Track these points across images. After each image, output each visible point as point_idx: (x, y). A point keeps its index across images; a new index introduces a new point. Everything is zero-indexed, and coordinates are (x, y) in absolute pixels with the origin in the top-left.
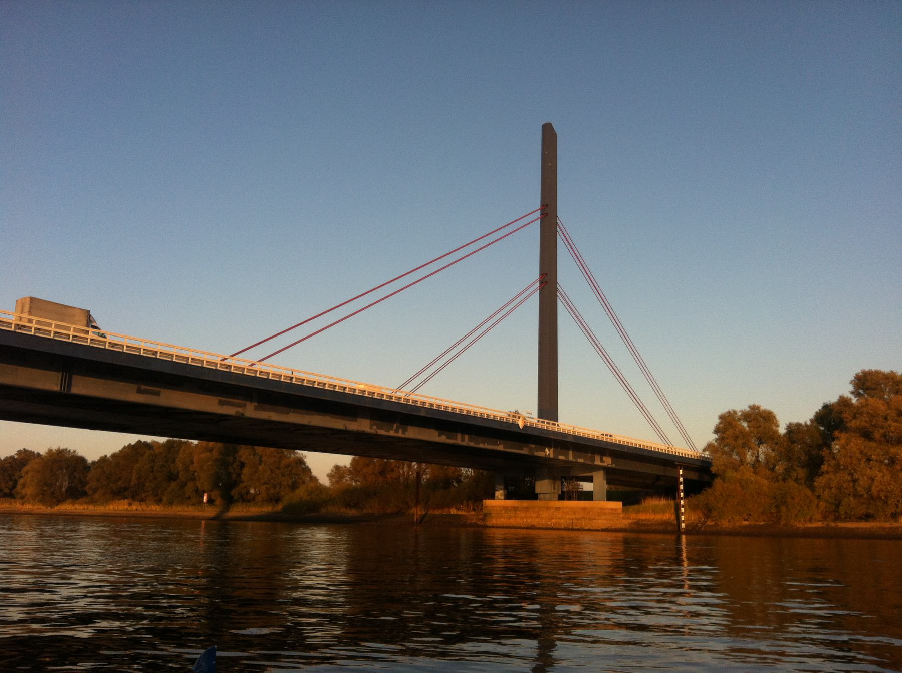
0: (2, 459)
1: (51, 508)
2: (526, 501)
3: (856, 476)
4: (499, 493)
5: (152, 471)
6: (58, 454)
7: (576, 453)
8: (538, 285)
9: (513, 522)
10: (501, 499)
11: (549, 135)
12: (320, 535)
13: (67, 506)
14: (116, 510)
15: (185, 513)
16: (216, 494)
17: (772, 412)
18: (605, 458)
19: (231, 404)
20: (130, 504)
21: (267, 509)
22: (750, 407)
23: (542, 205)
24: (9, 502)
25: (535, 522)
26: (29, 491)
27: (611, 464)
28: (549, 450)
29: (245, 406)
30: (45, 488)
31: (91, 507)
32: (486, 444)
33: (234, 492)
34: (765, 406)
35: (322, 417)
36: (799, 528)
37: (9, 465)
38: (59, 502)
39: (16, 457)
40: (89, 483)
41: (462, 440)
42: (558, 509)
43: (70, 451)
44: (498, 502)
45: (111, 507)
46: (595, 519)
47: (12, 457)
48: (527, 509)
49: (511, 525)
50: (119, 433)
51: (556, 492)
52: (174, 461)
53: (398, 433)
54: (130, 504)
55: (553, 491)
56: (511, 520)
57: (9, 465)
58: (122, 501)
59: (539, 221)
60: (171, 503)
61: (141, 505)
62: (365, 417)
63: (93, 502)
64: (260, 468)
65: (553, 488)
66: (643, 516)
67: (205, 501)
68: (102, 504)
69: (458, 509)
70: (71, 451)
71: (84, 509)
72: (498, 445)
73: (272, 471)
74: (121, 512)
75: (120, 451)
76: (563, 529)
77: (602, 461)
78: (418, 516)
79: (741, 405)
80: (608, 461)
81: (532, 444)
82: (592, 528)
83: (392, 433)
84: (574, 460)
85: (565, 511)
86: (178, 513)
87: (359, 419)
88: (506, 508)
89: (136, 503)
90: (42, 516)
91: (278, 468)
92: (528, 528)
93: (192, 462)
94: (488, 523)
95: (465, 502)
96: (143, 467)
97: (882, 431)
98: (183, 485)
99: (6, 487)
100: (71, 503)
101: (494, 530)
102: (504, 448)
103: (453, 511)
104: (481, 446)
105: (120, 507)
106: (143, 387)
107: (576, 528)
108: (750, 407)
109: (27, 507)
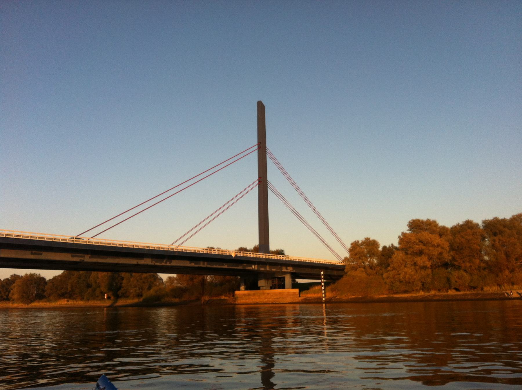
0: (2, 280)
1: (28, 305)
2: (253, 291)
3: (400, 272)
4: (242, 288)
5: (79, 284)
6: (30, 276)
7: (271, 266)
8: (257, 182)
9: (248, 301)
10: (243, 290)
11: (261, 108)
12: (163, 313)
13: (36, 304)
14: (61, 305)
15: (95, 305)
16: (110, 294)
17: (376, 241)
18: (288, 268)
19: (78, 256)
20: (68, 301)
21: (136, 300)
22: (365, 238)
23: (258, 143)
24: (6, 303)
25: (258, 301)
26: (15, 296)
27: (293, 271)
28: (254, 266)
29: (84, 257)
30: (24, 295)
31: (48, 304)
32: (217, 265)
33: (119, 293)
34: (372, 238)
35: (124, 259)
36: (376, 298)
37: (6, 283)
38: (32, 302)
39: (10, 278)
40: (46, 291)
41: (205, 265)
42: (268, 294)
43: (37, 274)
44: (242, 292)
45: (58, 303)
46: (285, 298)
47: (7, 279)
48: (254, 294)
49: (247, 303)
50: (41, 270)
51: (269, 285)
52: (89, 278)
53: (167, 264)
54: (68, 301)
55: (267, 285)
56: (247, 300)
57: (6, 283)
58: (64, 299)
59: (257, 151)
60: (88, 300)
61: (73, 301)
62: (149, 258)
63: (49, 301)
64: (131, 279)
65: (267, 283)
66: (309, 295)
67: (105, 298)
68: (54, 302)
69: (226, 296)
70: (38, 274)
71: (44, 304)
72: (224, 265)
73: (137, 281)
74: (63, 306)
75: (62, 273)
76: (271, 304)
77: (287, 269)
78: (204, 301)
79: (361, 238)
80: (290, 269)
81: (245, 263)
82: (284, 302)
83: (163, 264)
84: (270, 270)
85: (272, 294)
86: (92, 305)
87: (145, 259)
88: (244, 295)
89: (71, 300)
90: (23, 309)
91: (141, 279)
92: (255, 304)
93: (98, 278)
94: (236, 303)
95: (228, 293)
96: (74, 281)
97: (412, 250)
98: (94, 290)
99: (4, 295)
100: (38, 302)
101: (239, 306)
102: (228, 266)
103: (223, 297)
104: (215, 266)
105: (63, 302)
106: (34, 252)
107: (277, 303)
108: (365, 238)
109: (15, 305)
